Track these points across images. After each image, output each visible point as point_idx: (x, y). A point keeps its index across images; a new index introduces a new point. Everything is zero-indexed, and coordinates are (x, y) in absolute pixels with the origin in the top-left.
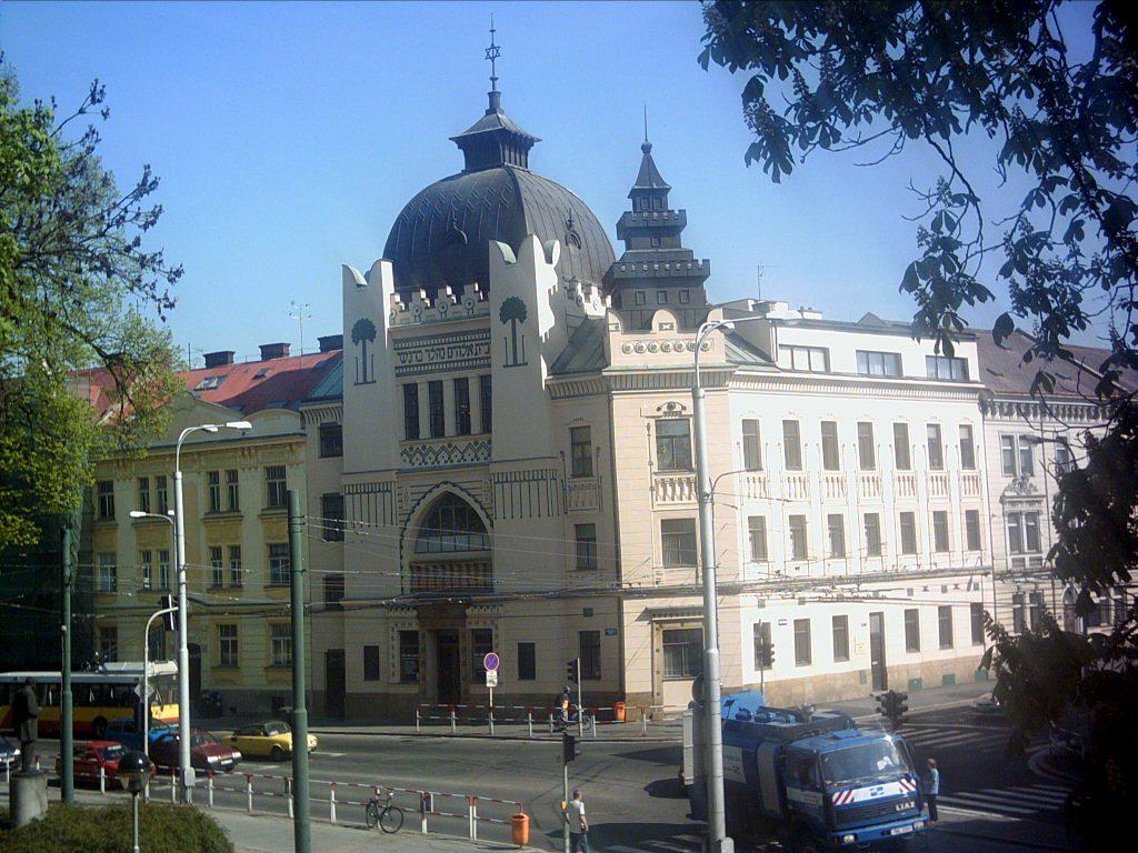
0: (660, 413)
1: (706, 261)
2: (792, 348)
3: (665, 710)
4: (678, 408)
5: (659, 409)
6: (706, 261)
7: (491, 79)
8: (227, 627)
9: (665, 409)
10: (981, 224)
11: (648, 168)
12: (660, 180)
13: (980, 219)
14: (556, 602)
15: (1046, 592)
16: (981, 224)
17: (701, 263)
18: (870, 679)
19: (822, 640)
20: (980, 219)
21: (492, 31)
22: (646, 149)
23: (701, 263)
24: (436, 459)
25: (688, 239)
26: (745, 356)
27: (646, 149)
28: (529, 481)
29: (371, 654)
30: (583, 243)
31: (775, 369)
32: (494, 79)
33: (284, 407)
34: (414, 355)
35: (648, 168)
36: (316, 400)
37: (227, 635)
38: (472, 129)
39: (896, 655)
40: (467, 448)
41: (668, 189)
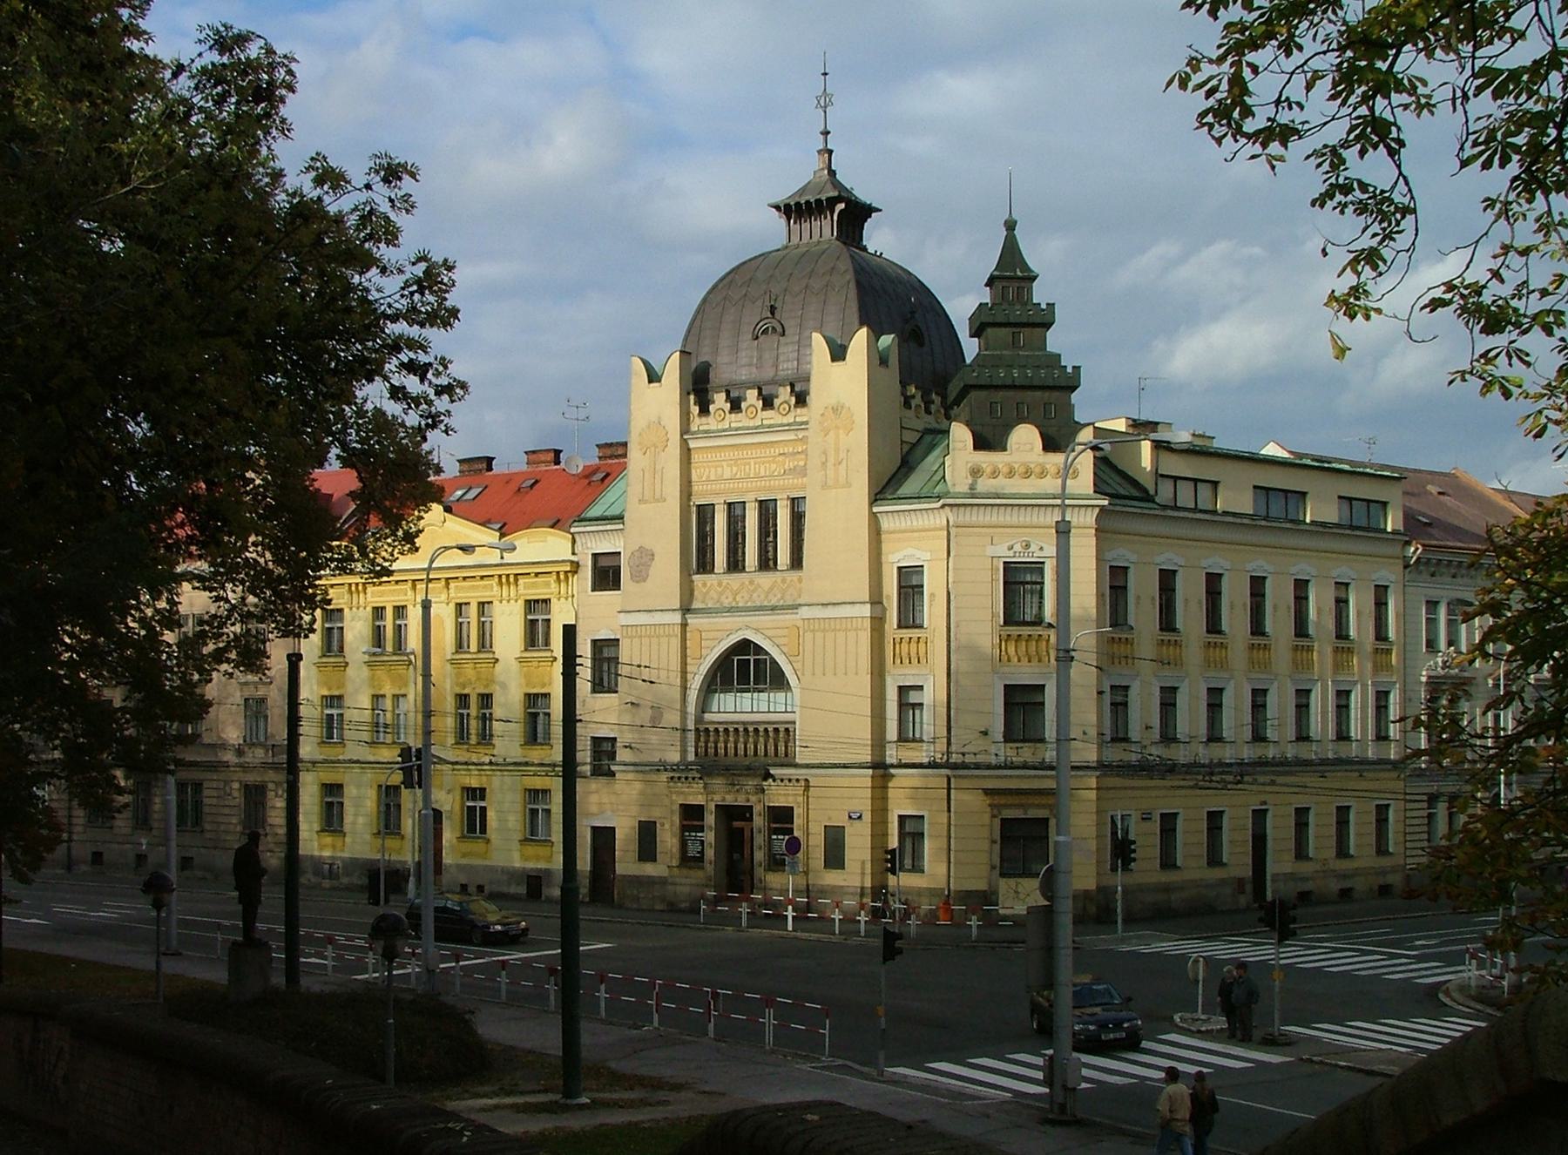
0: (1011, 553)
1: (1077, 369)
2: (1176, 479)
3: (1002, 912)
4: (1033, 548)
5: (1011, 548)
6: (1077, 369)
7: (822, 133)
8: (331, 785)
9: (1018, 548)
10: (1416, 235)
11: (1011, 253)
12: (1025, 267)
13: (1417, 230)
14: (1110, 786)
15: (80, 829)
16: (1416, 235)
17: (1069, 370)
18: (1249, 888)
19: (1191, 836)
20: (1417, 230)
21: (825, 74)
22: (1010, 226)
23: (1069, 370)
24: (734, 599)
25: (1055, 340)
26: (1118, 487)
27: (1010, 226)
28: (856, 630)
29: (647, 831)
30: (927, 341)
31: (1151, 505)
32: (826, 133)
33: (552, 527)
34: (713, 470)
35: (1011, 253)
36: (590, 520)
37: (474, 799)
38: (803, 191)
39: (1279, 862)
40: (771, 589)
41: (1034, 278)
